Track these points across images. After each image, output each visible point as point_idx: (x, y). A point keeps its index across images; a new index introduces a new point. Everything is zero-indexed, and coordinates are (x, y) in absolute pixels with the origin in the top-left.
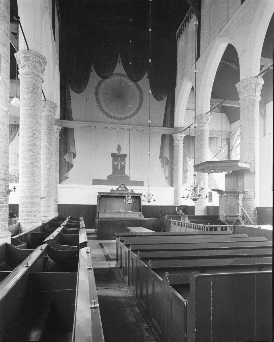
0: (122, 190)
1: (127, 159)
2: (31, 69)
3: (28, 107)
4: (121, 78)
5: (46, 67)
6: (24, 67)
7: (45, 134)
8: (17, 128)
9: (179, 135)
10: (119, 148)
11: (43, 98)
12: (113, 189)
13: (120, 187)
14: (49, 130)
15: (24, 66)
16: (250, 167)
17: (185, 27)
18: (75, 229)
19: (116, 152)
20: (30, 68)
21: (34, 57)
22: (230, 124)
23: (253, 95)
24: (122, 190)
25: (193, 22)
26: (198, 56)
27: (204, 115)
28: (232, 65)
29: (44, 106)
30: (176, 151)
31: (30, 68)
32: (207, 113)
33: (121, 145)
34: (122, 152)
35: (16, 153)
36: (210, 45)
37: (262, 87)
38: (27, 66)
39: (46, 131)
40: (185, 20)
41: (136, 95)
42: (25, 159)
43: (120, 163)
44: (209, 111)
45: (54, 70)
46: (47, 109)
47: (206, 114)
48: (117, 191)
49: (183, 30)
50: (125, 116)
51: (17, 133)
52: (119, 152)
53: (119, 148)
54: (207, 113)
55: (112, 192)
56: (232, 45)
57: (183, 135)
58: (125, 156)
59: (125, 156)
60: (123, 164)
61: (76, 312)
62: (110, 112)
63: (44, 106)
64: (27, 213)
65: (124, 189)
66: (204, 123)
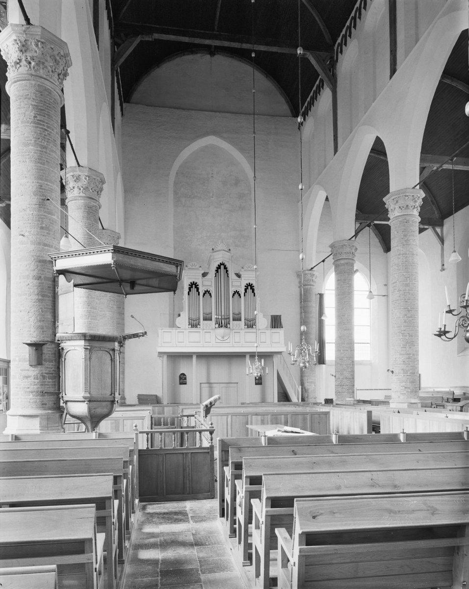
2: (34, 68)
5: (104, 185)
6: (18, 66)
11: (100, 227)
15: (18, 63)
17: (312, 106)
18: (125, 509)
20: (30, 67)
25: (326, 95)
26: (393, 71)
31: (30, 67)
32: (416, 186)
36: (311, 189)
37: (423, 201)
38: (24, 63)
40: (349, 25)
44: (418, 182)
45: (116, 179)
49: (346, 46)
54: (416, 186)
56: (380, 138)
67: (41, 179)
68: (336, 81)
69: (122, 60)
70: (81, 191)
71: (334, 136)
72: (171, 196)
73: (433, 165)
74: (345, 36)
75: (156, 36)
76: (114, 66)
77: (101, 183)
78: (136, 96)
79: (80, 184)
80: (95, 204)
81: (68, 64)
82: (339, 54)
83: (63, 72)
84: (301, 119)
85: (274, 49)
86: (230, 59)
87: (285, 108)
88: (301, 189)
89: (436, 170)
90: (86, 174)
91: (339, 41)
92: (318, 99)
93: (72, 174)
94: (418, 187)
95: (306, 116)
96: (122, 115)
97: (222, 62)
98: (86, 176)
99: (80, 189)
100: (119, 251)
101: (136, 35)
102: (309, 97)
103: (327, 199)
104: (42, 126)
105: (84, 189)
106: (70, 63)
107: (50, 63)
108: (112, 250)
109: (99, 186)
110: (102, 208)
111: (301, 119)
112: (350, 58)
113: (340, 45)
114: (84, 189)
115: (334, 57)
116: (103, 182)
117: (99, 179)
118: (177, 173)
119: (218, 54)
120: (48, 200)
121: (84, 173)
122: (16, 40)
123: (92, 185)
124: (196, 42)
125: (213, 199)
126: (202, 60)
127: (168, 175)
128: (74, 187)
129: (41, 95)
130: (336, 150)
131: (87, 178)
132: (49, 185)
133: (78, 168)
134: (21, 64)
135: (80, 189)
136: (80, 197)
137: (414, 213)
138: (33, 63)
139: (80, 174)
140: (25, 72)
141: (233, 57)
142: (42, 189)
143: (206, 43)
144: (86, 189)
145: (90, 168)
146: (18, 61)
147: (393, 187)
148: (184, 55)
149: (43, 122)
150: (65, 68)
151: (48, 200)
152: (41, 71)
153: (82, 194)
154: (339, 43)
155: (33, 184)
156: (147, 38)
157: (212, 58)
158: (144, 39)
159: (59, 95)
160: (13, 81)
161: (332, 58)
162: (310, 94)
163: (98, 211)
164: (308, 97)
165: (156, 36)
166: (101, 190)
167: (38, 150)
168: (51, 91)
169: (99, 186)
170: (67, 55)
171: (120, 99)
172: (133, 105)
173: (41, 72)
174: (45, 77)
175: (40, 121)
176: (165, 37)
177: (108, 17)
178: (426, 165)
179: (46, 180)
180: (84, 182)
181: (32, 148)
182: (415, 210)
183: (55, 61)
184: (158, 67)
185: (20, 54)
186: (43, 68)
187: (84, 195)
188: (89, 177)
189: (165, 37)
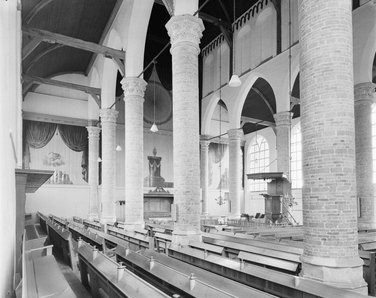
0: (160, 191)
1: (162, 162)
3: (136, 125)
4: (162, 88)
7: (109, 140)
8: (55, 126)
9: (206, 141)
10: (155, 153)
12: (151, 190)
13: (158, 188)
14: (112, 136)
16: (287, 178)
19: (152, 155)
21: (142, 84)
22: (244, 135)
23: (287, 125)
24: (160, 191)
27: (238, 130)
28: (255, 90)
29: (109, 113)
30: (203, 156)
33: (156, 148)
34: (158, 155)
35: (55, 153)
38: (135, 90)
39: (110, 137)
41: (169, 105)
42: (135, 170)
43: (156, 166)
46: (111, 116)
47: (110, 108)
48: (155, 192)
50: (159, 121)
51: (55, 132)
52: (155, 155)
53: (155, 153)
55: (151, 193)
56: (264, 80)
57: (209, 142)
58: (160, 159)
59: (160, 159)
60: (158, 166)
61: (212, 288)
62: (146, 117)
63: (109, 113)
64: (137, 216)
65: (161, 190)
66: (237, 136)
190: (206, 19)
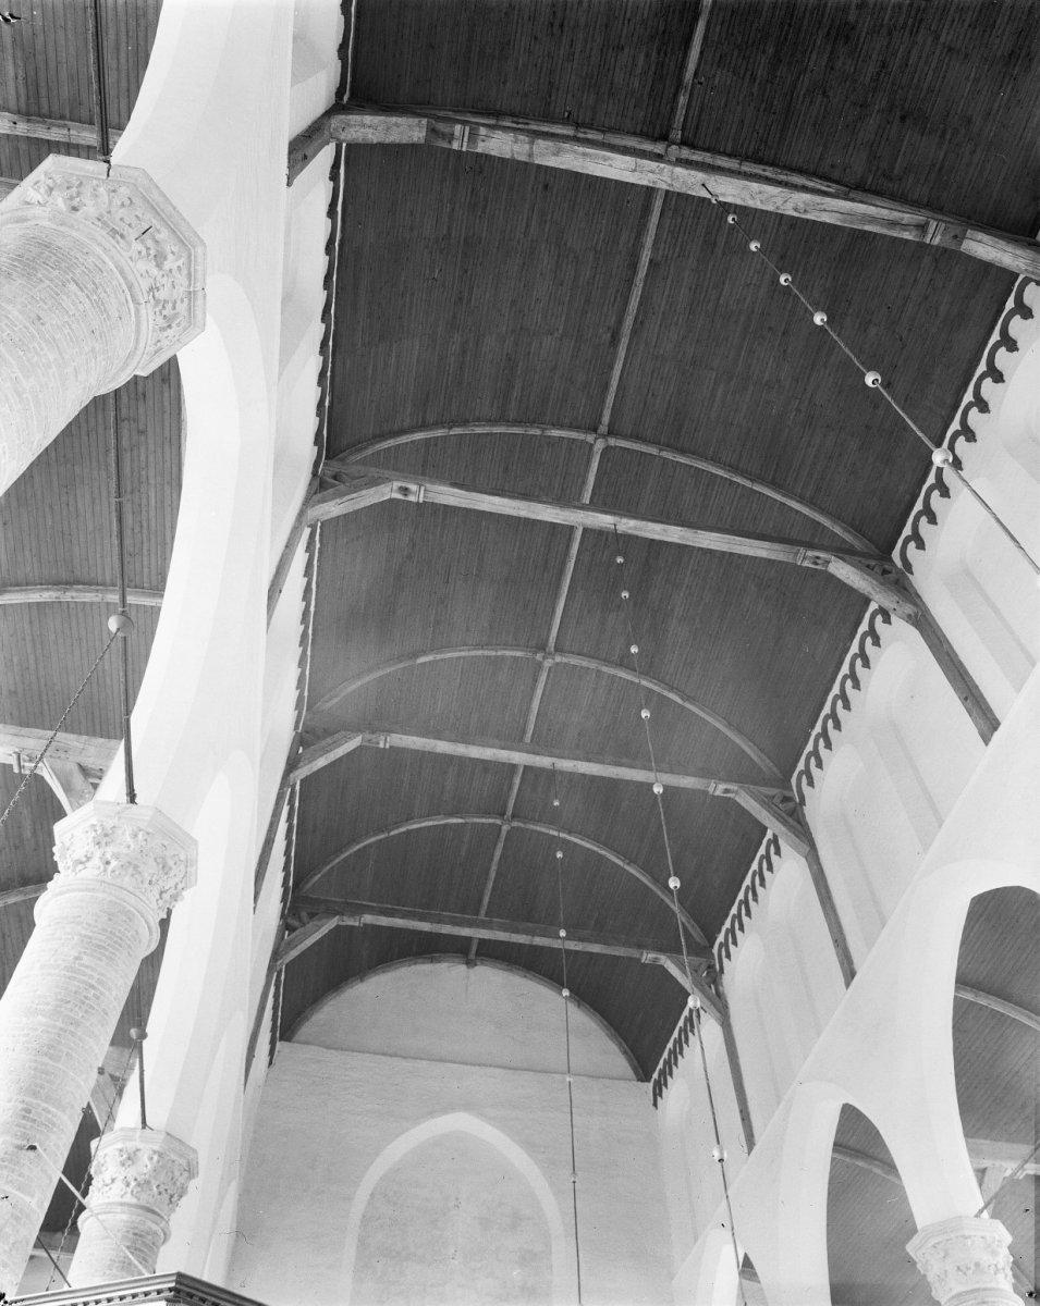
20: (105, 871)
26: (850, 974)
31: (105, 871)
44: (982, 1205)
67: (35, 1094)
68: (726, 1006)
69: (294, 954)
70: (129, 1190)
71: (741, 1111)
72: (350, 1251)
73: (1003, 1164)
74: (732, 931)
75: (368, 919)
76: (277, 960)
77: (186, 1174)
78: (306, 1030)
79: (131, 1172)
80: (154, 1227)
81: (187, 880)
82: (725, 960)
83: (172, 891)
84: (696, 1001)
85: (596, 948)
86: (506, 974)
87: (619, 1062)
88: (721, 1160)
89: (1011, 1176)
90: (156, 1148)
91: (721, 938)
92: (664, 1095)
93: (120, 1146)
94: (985, 1214)
95: (664, 1088)
96: (270, 1063)
97: (491, 981)
98: (155, 1152)
99: (128, 1185)
100: (191, 1296)
101: (331, 913)
102: (661, 1062)
103: (747, 1267)
104: (85, 978)
105: (139, 1185)
106: (193, 878)
107: (150, 869)
108: (170, 1290)
109: (182, 1180)
110: (172, 1241)
111: (696, 1001)
112: (747, 962)
113: (725, 945)
114: (139, 1185)
115: (714, 965)
116: (191, 1171)
117: (183, 1162)
118: (372, 1195)
119: (482, 964)
120: (33, 1148)
121: (147, 1147)
122: (93, 825)
123: (162, 1178)
124: (443, 931)
125: (456, 1262)
126: (449, 975)
127: (349, 1199)
128: (113, 1180)
129: (110, 920)
130: (850, 974)
131: (156, 1157)
132: (49, 1112)
133: (139, 1132)
134: (89, 864)
135: (128, 1185)
136: (122, 1204)
137: (1001, 1286)
138: (114, 863)
139: (141, 1146)
140: (91, 877)
141: (511, 970)
142: (28, 1119)
143: (463, 934)
144: (143, 1185)
145: (168, 1134)
146: (84, 859)
147: (922, 1218)
148: (415, 964)
149: (93, 969)
150: (180, 886)
151: (33, 1148)
152: (127, 879)
153: (129, 1199)
154: (721, 943)
155: (9, 1105)
156: (350, 922)
157: (471, 971)
158: (344, 923)
159: (149, 927)
160: (57, 891)
161: (711, 967)
162: (657, 1066)
163: (158, 1248)
164: (668, 1041)
165: (368, 919)
166: (182, 1192)
167: (54, 1027)
168: (134, 915)
169: (182, 1180)
170: (189, 863)
171: (273, 1030)
172: (296, 1045)
173: (127, 881)
174: (130, 889)
175: (87, 967)
176: (384, 921)
177: (284, 883)
178: (986, 1163)
179: (48, 1099)
180: (145, 1165)
181: (44, 1020)
182: (1001, 1276)
183: (163, 867)
184: (362, 981)
185: (92, 848)
186: (132, 875)
187: (134, 1201)
188: (160, 1155)
189: (384, 921)
190: (530, 155)
